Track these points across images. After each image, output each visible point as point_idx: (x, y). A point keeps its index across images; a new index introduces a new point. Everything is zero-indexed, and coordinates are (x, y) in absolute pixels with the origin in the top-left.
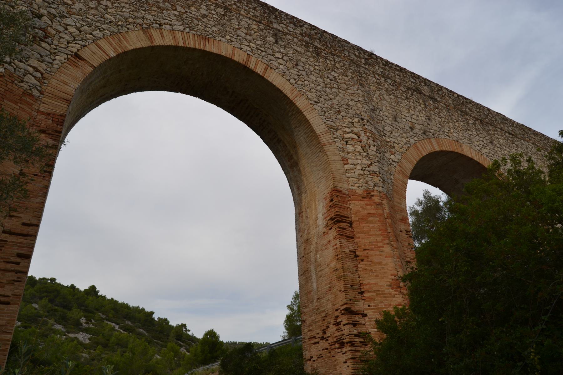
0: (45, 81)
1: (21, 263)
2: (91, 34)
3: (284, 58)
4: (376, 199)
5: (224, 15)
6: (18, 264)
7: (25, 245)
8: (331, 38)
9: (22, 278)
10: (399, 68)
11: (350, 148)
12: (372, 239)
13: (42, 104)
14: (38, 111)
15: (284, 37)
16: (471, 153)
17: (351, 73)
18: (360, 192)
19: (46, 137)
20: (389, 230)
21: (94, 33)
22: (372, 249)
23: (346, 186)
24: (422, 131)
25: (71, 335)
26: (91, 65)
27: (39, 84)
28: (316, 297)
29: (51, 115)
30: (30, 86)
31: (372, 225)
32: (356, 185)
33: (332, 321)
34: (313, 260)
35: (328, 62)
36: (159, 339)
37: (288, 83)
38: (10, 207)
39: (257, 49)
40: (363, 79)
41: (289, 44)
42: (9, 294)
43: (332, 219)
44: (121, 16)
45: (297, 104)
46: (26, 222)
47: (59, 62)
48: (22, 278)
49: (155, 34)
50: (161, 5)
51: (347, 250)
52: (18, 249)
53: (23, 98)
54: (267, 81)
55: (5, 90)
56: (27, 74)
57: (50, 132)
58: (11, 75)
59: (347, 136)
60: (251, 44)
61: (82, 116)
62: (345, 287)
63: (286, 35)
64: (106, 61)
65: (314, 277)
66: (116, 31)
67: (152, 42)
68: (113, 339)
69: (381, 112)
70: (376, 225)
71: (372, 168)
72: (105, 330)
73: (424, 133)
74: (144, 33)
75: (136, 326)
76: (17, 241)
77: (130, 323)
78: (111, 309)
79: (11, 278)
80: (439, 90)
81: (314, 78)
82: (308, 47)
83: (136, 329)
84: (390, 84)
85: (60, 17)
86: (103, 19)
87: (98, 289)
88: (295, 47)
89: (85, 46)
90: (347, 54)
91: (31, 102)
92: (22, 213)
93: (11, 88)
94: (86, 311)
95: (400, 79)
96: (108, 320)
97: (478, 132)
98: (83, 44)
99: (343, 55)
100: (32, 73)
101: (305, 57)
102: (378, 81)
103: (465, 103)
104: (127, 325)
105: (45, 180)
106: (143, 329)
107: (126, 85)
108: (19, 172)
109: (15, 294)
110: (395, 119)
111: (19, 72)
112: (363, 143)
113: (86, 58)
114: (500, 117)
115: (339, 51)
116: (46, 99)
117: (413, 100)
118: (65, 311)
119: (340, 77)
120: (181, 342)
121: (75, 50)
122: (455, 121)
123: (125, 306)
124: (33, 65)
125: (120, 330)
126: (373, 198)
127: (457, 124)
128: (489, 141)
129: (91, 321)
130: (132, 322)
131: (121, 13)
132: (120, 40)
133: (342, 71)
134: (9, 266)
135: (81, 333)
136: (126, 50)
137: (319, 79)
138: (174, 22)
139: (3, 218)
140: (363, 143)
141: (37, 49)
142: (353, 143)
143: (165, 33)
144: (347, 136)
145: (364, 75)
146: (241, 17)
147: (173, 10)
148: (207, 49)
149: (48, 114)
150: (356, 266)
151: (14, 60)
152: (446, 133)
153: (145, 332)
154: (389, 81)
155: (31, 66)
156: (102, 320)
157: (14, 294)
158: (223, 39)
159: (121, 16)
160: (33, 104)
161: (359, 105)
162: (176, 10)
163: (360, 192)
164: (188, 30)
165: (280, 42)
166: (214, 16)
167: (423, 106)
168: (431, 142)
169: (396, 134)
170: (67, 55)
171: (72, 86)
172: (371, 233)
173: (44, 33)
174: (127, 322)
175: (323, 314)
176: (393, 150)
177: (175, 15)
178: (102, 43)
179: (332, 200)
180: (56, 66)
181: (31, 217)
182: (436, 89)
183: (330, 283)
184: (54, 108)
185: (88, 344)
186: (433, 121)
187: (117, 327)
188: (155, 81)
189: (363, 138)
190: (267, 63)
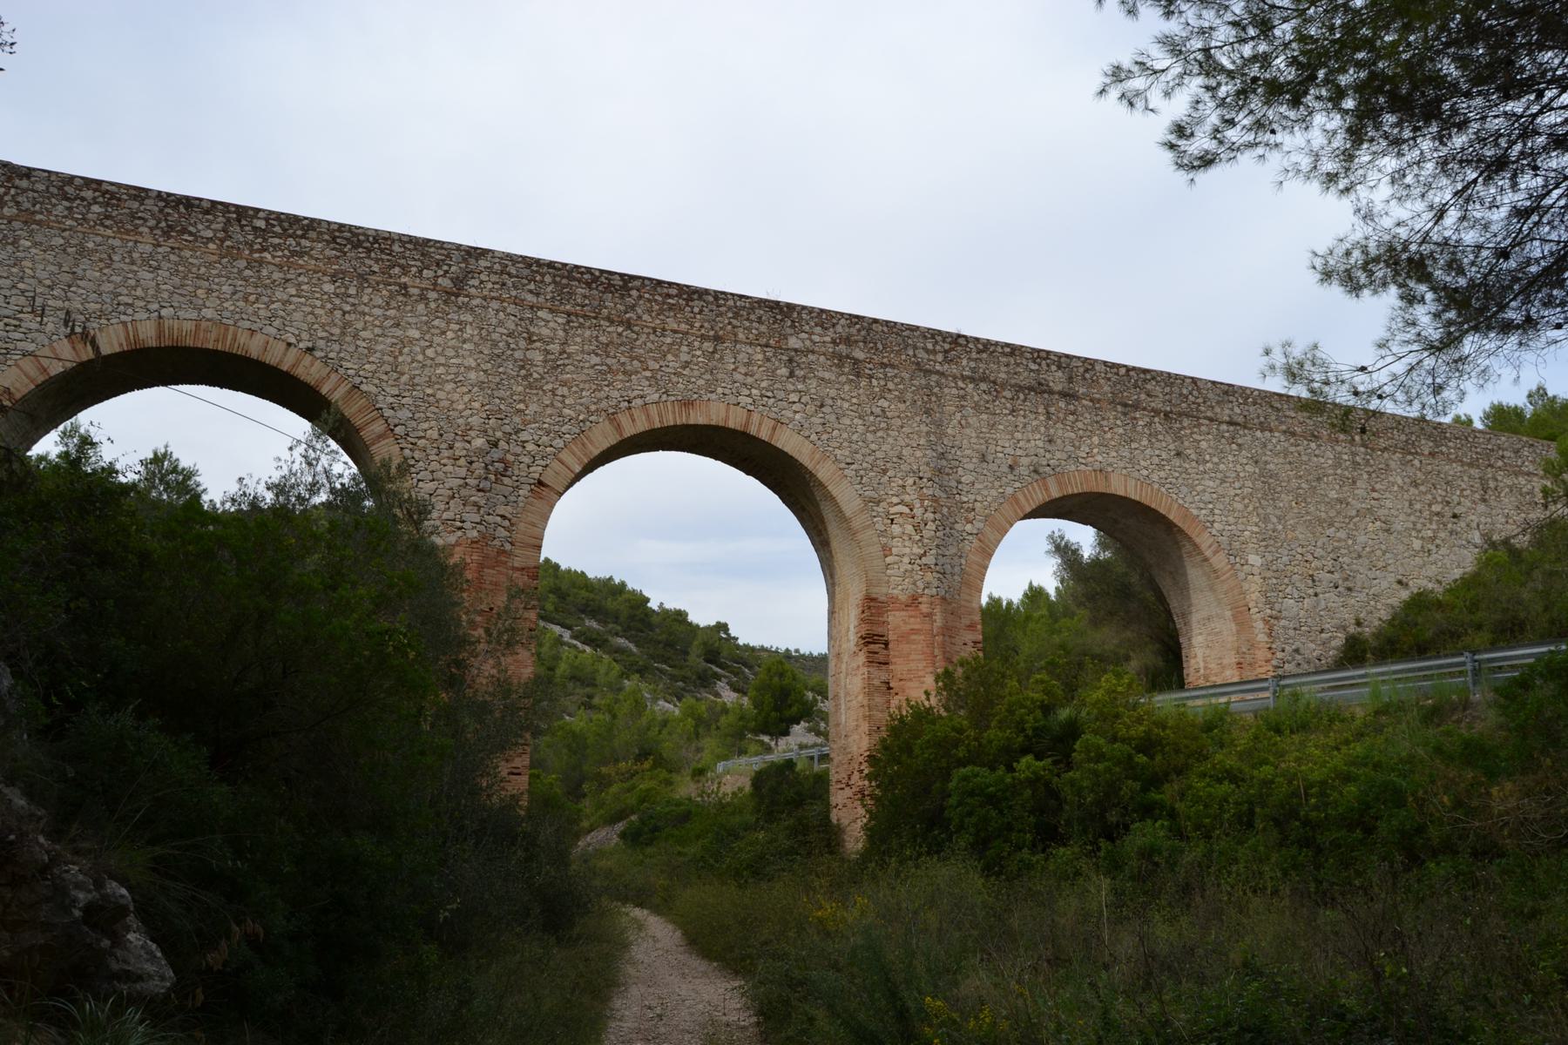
2: (551, 446)
4: (924, 608)
5: (713, 352)
8: (885, 329)
10: (1008, 350)
11: (896, 529)
12: (913, 665)
14: (514, 569)
15: (804, 359)
16: (1126, 487)
18: (903, 598)
20: (937, 652)
22: (911, 680)
23: (884, 590)
24: (1032, 468)
28: (844, 733)
31: (914, 646)
32: (900, 587)
33: (857, 767)
34: (843, 684)
35: (875, 382)
36: (665, 662)
37: (807, 442)
40: (934, 399)
44: (582, 405)
45: (820, 475)
49: (624, 419)
54: (776, 447)
59: (893, 510)
62: (870, 730)
65: (843, 707)
66: (577, 431)
67: (621, 435)
68: (562, 668)
70: (920, 647)
71: (924, 560)
75: (610, 632)
77: (594, 624)
78: (550, 592)
80: (1087, 370)
83: (610, 638)
84: (984, 391)
86: (561, 419)
88: (820, 374)
89: (547, 466)
90: (911, 352)
97: (1153, 440)
99: (903, 357)
102: (962, 392)
104: (589, 629)
106: (627, 638)
112: (916, 520)
114: (1218, 391)
117: (1025, 411)
119: (893, 407)
120: (717, 666)
122: (1107, 429)
125: (575, 642)
126: (921, 606)
127: (1109, 436)
128: (1172, 453)
130: (599, 621)
131: (582, 400)
132: (583, 444)
137: (856, 421)
138: (647, 391)
140: (916, 520)
142: (901, 520)
143: (636, 413)
144: (893, 510)
147: (644, 370)
150: (889, 702)
152: (1080, 460)
153: (632, 646)
154: (983, 386)
158: (713, 396)
159: (582, 405)
161: (919, 454)
163: (903, 598)
166: (700, 359)
167: (1042, 418)
168: (1045, 485)
169: (980, 486)
172: (912, 657)
174: (587, 623)
175: (850, 756)
176: (971, 516)
177: (647, 378)
179: (863, 612)
180: (521, 504)
182: (1081, 370)
183: (857, 720)
186: (1059, 441)
187: (567, 635)
189: (918, 511)
190: (776, 416)
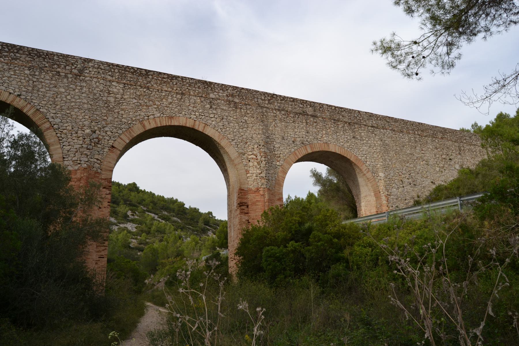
2: (117, 133)
3: (215, 117)
4: (261, 193)
5: (181, 99)
8: (246, 91)
11: (251, 164)
14: (102, 179)
15: (216, 102)
17: (257, 114)
18: (253, 189)
21: (118, 132)
23: (246, 186)
25: (122, 225)
28: (233, 240)
36: (190, 225)
37: (217, 132)
39: (200, 115)
41: (219, 106)
42: (103, 254)
43: (238, 204)
49: (146, 123)
50: (148, 104)
51: (244, 220)
59: (250, 157)
60: (197, 113)
63: (217, 101)
67: (145, 129)
68: (154, 228)
69: (274, 136)
72: (147, 220)
73: (302, 143)
75: (171, 216)
77: (166, 213)
78: (151, 202)
80: (320, 107)
81: (233, 125)
82: (229, 104)
83: (171, 218)
87: (138, 185)
88: (222, 107)
89: (115, 140)
94: (131, 205)
95: (292, 108)
96: (148, 211)
98: (114, 139)
99: (253, 102)
101: (228, 112)
103: (340, 112)
110: (283, 138)
115: (251, 99)
118: (115, 205)
121: (111, 144)
123: (161, 199)
125: (159, 219)
129: (136, 213)
130: (168, 212)
131: (129, 116)
133: (251, 115)
135: (129, 223)
142: (252, 161)
143: (151, 121)
144: (250, 157)
145: (265, 114)
146: (190, 97)
148: (173, 124)
149: (106, 179)
154: (283, 112)
156: (144, 212)
158: (181, 115)
161: (259, 136)
162: (155, 104)
164: (162, 115)
165: (213, 107)
166: (176, 101)
168: (306, 148)
174: (163, 213)
177: (155, 108)
178: (122, 136)
180: (105, 155)
185: (135, 232)
187: (156, 217)
189: (259, 157)
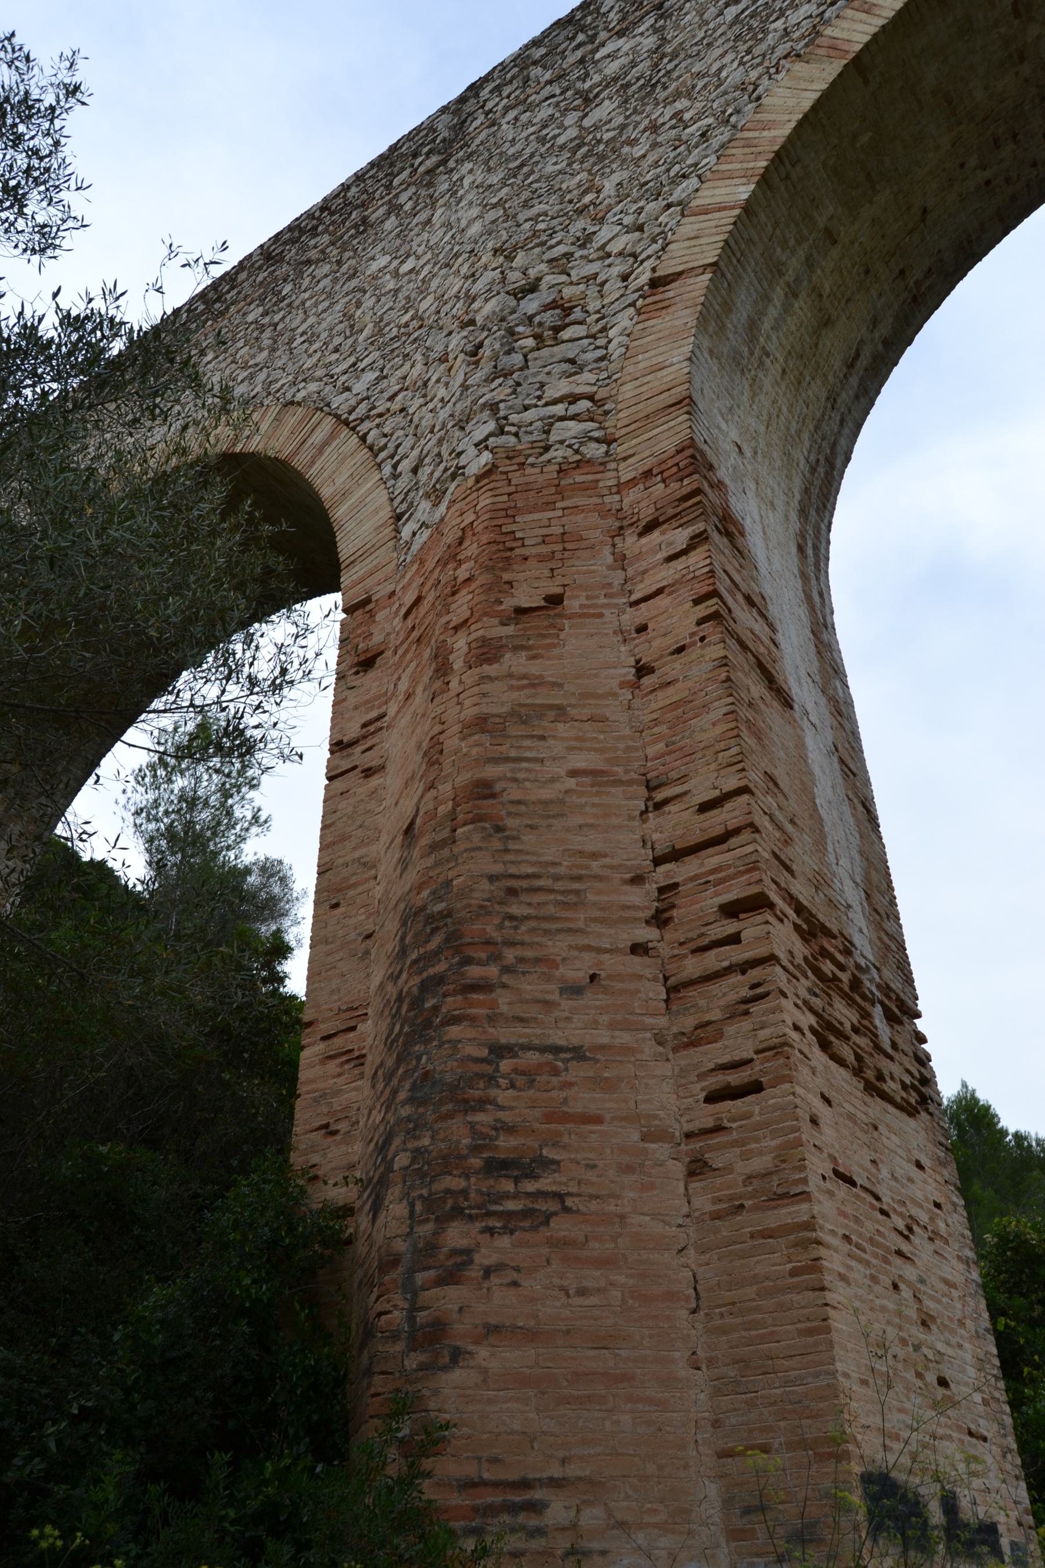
0: (606, 407)
1: (743, 935)
6: (734, 939)
7: (732, 871)
9: (765, 981)
13: (622, 465)
14: (620, 488)
19: (663, 533)
26: (701, 270)
27: (593, 425)
29: (655, 472)
30: (570, 446)
38: (648, 781)
46: (707, 799)
47: (621, 338)
48: (765, 981)
52: (717, 894)
53: (563, 483)
55: (509, 494)
56: (551, 424)
57: (671, 512)
58: (511, 455)
61: (838, 463)
64: (735, 223)
74: (807, 62)
76: (703, 870)
79: (732, 997)
85: (583, 246)
91: (590, 477)
92: (683, 778)
93: (523, 480)
100: (563, 413)
105: (709, 644)
107: (902, 272)
108: (633, 670)
109: (765, 1045)
111: (531, 433)
113: (680, 268)
116: (625, 446)
124: (558, 395)
134: (714, 960)
136: (776, 148)
139: (637, 823)
141: (552, 356)
149: (648, 474)
151: (505, 418)
155: (555, 402)
157: (761, 1047)
160: (597, 481)
170: (633, 304)
171: (675, 360)
173: (558, 311)
181: (716, 774)
184: (655, 449)
188: (988, 183)
